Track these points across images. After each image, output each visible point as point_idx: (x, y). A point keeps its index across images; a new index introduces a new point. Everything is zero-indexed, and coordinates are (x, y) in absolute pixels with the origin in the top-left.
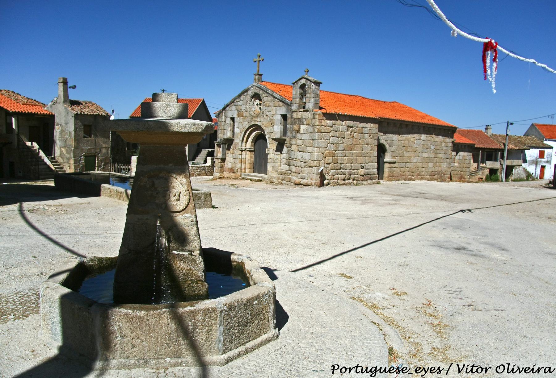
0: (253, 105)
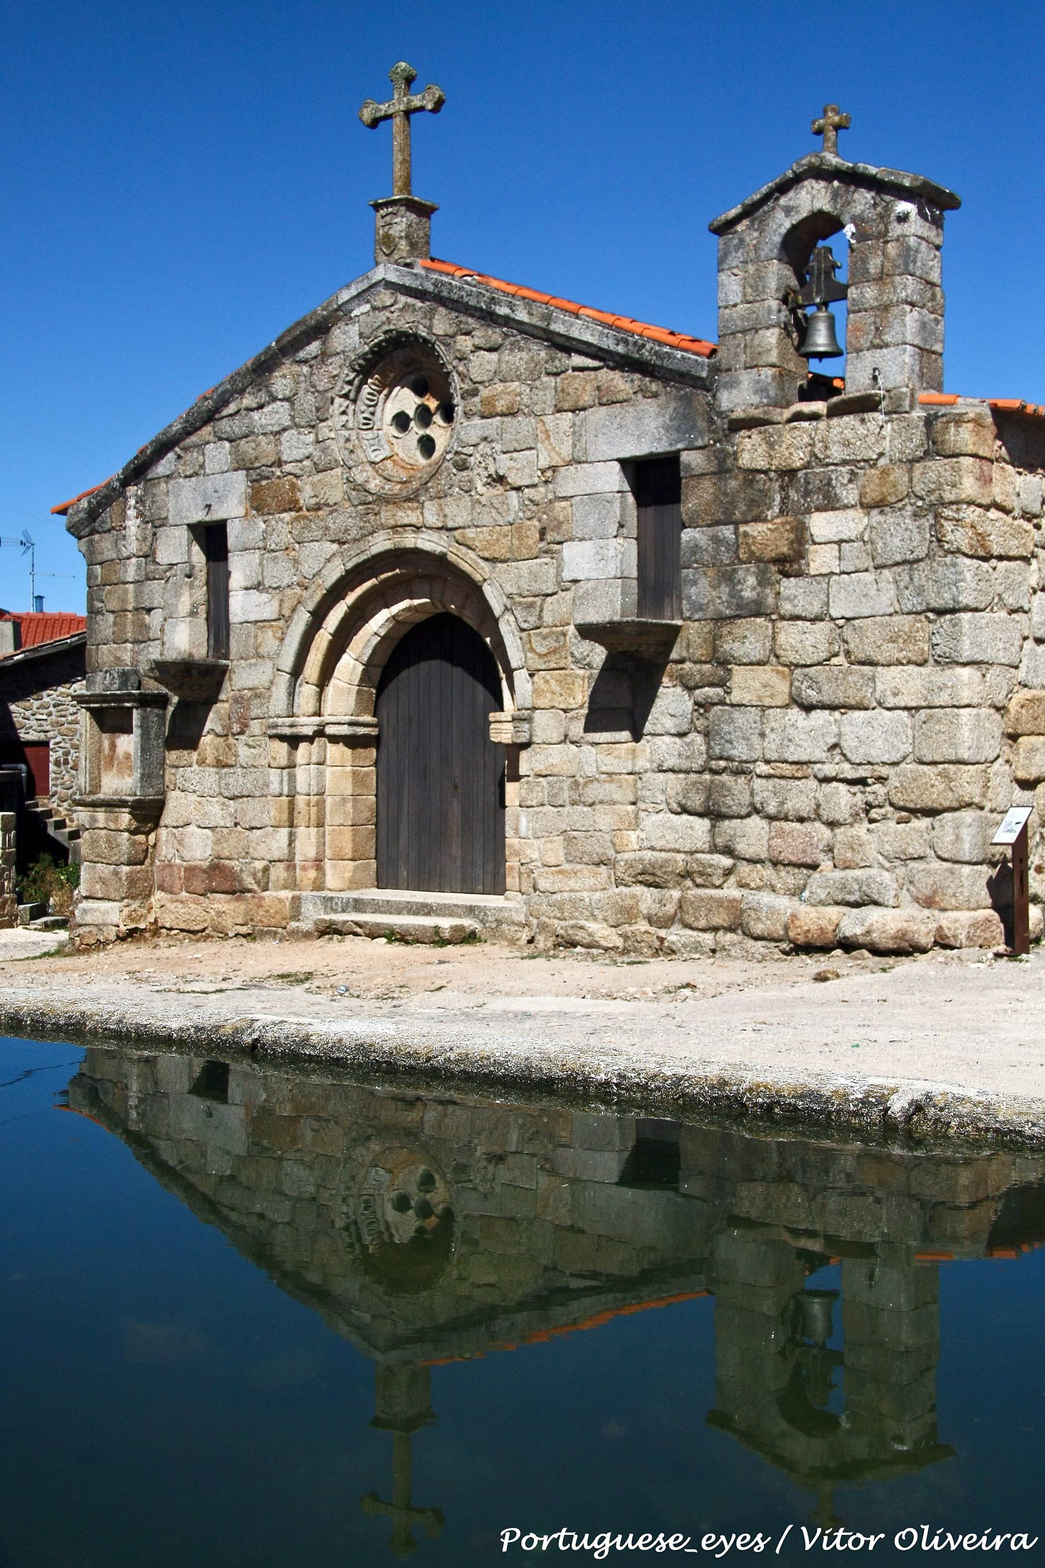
0: (368, 424)
